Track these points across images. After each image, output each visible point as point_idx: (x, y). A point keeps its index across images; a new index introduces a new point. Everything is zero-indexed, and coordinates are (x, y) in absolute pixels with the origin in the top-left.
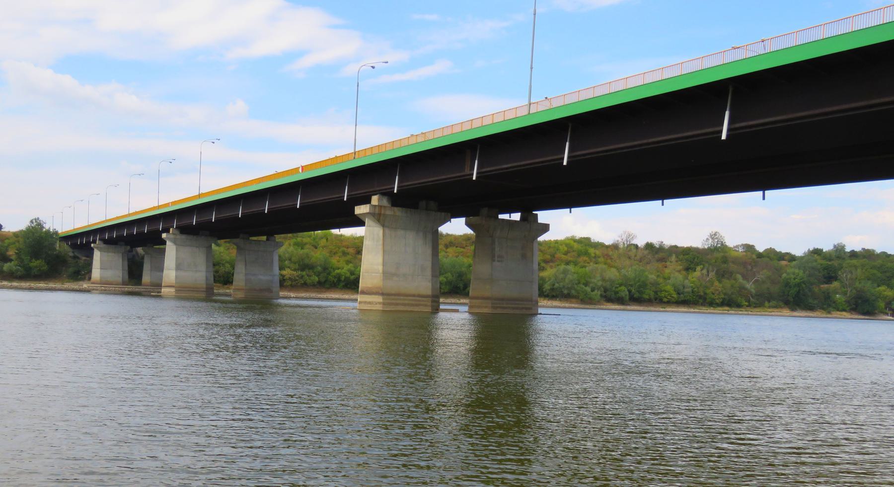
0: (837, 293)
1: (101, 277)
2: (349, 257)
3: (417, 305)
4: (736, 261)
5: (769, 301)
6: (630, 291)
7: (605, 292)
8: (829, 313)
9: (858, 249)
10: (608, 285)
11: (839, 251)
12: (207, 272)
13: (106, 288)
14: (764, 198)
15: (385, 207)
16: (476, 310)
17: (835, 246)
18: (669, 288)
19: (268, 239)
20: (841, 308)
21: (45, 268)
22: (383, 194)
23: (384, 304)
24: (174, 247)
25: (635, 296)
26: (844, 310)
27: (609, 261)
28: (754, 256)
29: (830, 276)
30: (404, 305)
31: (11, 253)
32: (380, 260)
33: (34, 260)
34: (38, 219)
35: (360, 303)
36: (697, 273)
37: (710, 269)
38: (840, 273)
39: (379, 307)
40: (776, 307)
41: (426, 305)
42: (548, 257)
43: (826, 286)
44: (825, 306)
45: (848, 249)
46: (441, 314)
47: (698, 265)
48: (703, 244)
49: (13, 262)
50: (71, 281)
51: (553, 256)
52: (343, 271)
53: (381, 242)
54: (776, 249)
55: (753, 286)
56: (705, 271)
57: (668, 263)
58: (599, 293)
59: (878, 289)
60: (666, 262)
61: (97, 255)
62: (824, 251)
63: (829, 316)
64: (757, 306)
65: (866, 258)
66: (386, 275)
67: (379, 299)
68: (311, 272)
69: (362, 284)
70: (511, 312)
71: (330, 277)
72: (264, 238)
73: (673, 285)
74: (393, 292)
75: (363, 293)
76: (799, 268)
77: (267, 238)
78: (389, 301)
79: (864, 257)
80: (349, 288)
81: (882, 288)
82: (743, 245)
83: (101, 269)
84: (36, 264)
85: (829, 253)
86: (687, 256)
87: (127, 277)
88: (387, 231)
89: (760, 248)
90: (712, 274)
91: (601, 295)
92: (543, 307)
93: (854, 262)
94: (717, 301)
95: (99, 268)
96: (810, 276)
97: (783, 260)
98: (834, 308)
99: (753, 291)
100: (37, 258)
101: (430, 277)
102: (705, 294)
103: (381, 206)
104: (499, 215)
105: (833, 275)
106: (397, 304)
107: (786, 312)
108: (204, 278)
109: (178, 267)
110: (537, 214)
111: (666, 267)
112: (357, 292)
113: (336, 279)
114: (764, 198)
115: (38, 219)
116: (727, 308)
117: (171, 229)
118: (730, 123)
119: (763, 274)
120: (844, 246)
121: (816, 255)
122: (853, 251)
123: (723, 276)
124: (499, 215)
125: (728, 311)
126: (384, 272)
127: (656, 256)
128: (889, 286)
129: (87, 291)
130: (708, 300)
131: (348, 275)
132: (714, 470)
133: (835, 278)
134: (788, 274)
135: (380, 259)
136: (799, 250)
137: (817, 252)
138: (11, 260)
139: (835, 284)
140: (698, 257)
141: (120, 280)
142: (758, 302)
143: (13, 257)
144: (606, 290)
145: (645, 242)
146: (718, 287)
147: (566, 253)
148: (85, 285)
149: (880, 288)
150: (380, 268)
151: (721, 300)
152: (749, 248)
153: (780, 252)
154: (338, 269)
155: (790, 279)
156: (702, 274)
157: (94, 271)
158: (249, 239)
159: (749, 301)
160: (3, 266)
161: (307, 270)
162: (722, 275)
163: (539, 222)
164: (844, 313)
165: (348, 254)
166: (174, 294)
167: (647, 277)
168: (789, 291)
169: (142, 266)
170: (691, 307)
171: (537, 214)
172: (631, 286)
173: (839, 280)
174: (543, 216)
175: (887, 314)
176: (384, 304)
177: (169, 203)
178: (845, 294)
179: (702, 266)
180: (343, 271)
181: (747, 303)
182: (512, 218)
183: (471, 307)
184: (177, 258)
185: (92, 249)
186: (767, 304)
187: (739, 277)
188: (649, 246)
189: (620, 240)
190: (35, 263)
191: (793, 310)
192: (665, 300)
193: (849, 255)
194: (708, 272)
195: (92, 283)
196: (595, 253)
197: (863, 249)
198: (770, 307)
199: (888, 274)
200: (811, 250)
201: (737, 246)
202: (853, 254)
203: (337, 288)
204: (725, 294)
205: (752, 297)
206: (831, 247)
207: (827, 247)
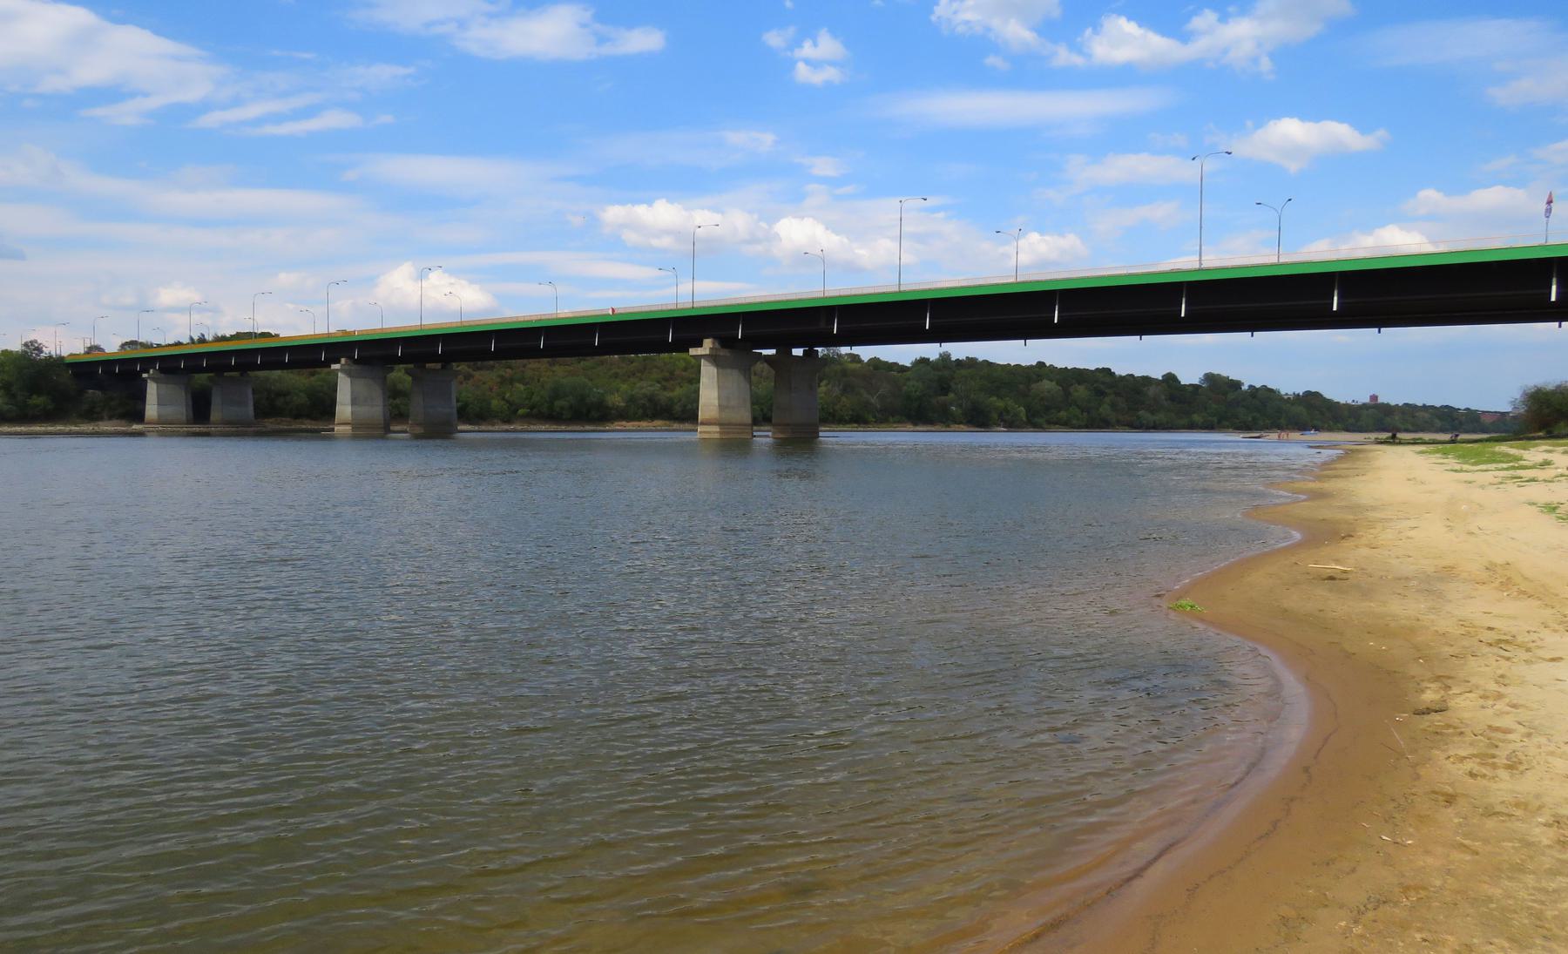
0: (952, 405)
1: (159, 416)
3: (741, 433)
5: (893, 416)
6: (762, 410)
8: (948, 426)
12: (384, 406)
13: (167, 428)
16: (776, 436)
17: (940, 355)
19: (443, 367)
23: (720, 433)
24: (348, 380)
26: (961, 423)
29: (944, 388)
32: (716, 394)
33: (35, 396)
34: (36, 342)
35: (701, 432)
38: (952, 384)
40: (899, 422)
42: (667, 374)
43: (943, 398)
44: (944, 420)
45: (953, 359)
50: (86, 421)
51: (672, 373)
53: (716, 379)
63: (948, 429)
66: (721, 407)
67: (716, 429)
72: (439, 366)
75: (702, 424)
88: (721, 370)
93: (964, 372)
104: (793, 350)
107: (910, 427)
109: (354, 402)
112: (334, 424)
116: (856, 425)
118: (1059, 313)
120: (950, 355)
124: (793, 350)
129: (140, 434)
132: (243, 775)
135: (715, 394)
139: (951, 395)
141: (184, 418)
147: (685, 369)
148: (136, 427)
150: (716, 402)
157: (148, 407)
159: (875, 417)
162: (847, 389)
163: (866, 361)
164: (962, 426)
175: (999, 425)
176: (720, 433)
178: (960, 406)
181: (874, 420)
183: (774, 433)
184: (352, 392)
185: (145, 381)
186: (891, 419)
190: (38, 400)
191: (915, 424)
197: (967, 358)
198: (895, 422)
204: (853, 410)
206: (938, 356)
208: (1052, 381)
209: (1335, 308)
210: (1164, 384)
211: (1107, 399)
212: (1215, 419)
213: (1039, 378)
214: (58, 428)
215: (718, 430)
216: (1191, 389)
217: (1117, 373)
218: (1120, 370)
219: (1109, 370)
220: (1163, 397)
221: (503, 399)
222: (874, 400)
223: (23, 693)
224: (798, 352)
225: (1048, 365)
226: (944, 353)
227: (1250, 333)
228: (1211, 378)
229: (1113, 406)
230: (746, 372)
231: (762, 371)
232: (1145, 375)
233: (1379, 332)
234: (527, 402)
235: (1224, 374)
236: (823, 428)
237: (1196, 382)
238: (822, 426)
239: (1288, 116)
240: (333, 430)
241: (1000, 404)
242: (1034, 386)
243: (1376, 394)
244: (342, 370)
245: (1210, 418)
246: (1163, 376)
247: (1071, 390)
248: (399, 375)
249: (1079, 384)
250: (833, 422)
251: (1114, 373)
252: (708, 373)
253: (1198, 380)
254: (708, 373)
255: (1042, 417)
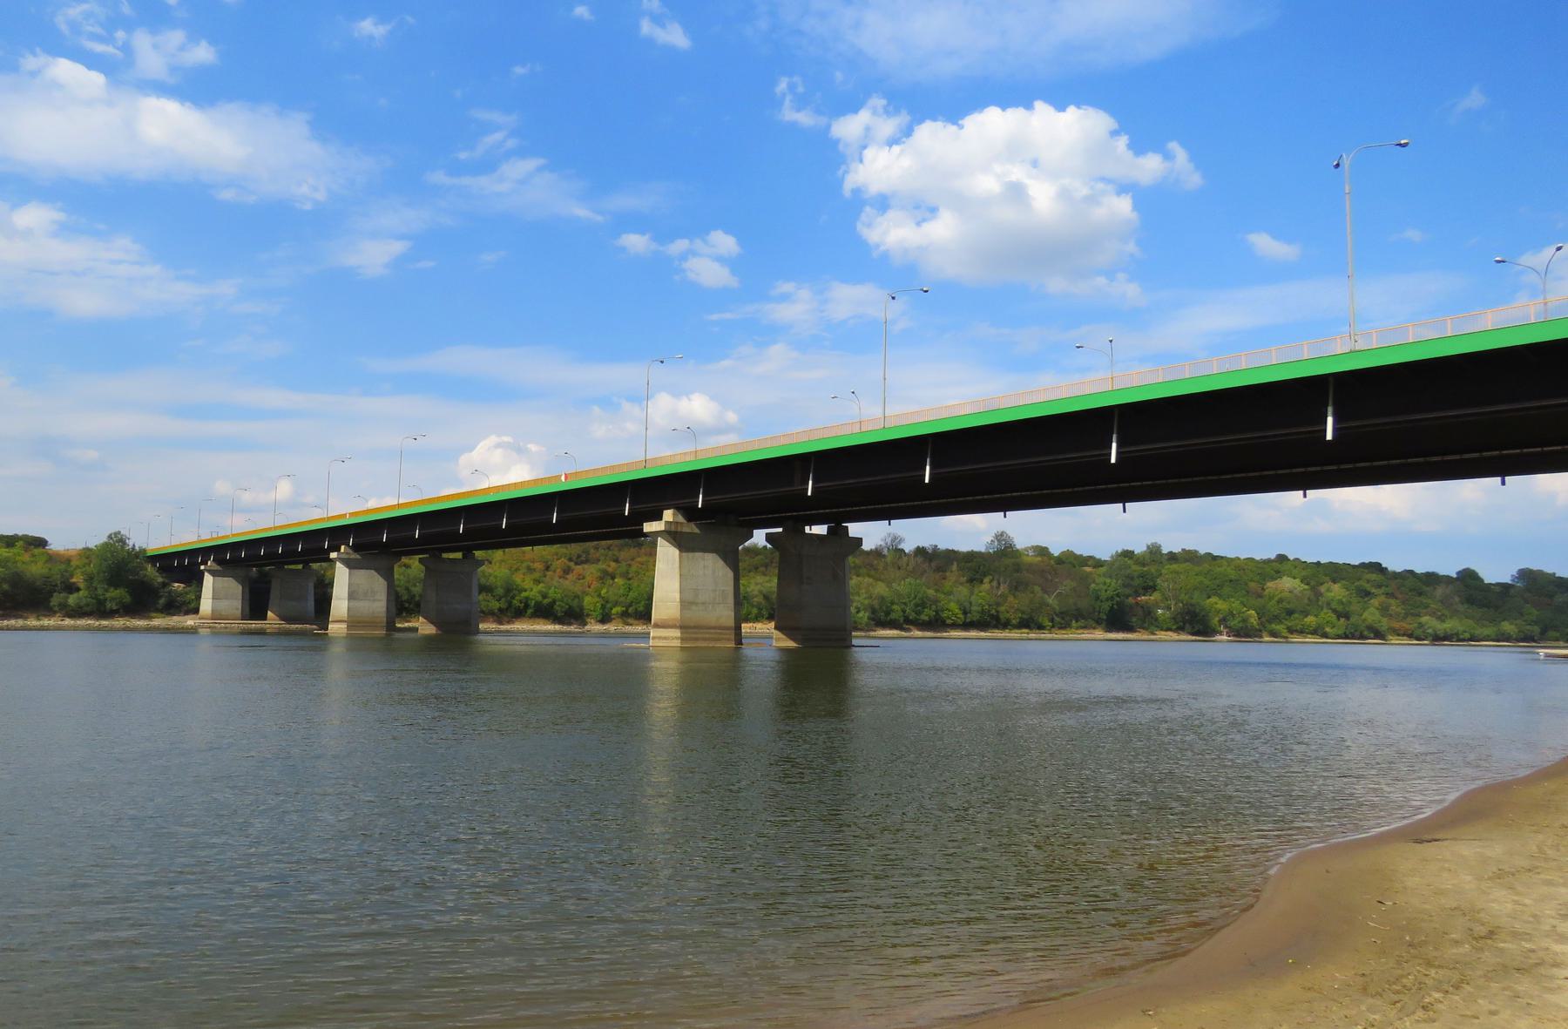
2: (537, 575)
3: (719, 640)
4: (1030, 568)
6: (904, 611)
7: (873, 613)
9: (1177, 550)
10: (876, 603)
11: (1154, 551)
14: (1125, 511)
15: (681, 523)
17: (1148, 547)
18: (953, 606)
19: (465, 556)
20: (1165, 627)
21: (128, 599)
22: (678, 508)
25: (911, 618)
26: (1168, 629)
27: (873, 573)
28: (1052, 562)
30: (705, 639)
31: (78, 579)
34: (119, 532)
35: (654, 638)
36: (986, 586)
37: (1001, 580)
38: (1159, 581)
39: (677, 643)
41: (729, 640)
45: (1165, 551)
46: (481, 637)
47: (985, 576)
48: (987, 548)
49: (81, 593)
52: (532, 593)
54: (1076, 552)
55: (1056, 602)
56: (995, 584)
57: (948, 574)
58: (867, 614)
59: (1208, 601)
60: (946, 571)
61: (208, 580)
62: (1136, 553)
63: (1153, 637)
64: (1064, 626)
65: (1188, 561)
66: (685, 604)
68: (489, 597)
69: (656, 615)
70: (704, 644)
71: (515, 602)
73: (958, 602)
74: (692, 624)
75: (657, 626)
76: (1110, 577)
77: (463, 555)
78: (688, 636)
79: (1186, 561)
80: (538, 617)
81: (1214, 599)
82: (1033, 547)
83: (213, 599)
84: (116, 594)
85: (1143, 555)
86: (970, 564)
87: (247, 609)
89: (1056, 551)
90: (1003, 589)
91: (869, 618)
92: (857, 637)
94: (1014, 622)
95: (211, 597)
96: (1125, 586)
97: (1087, 565)
98: (1157, 627)
99: (1057, 608)
100: (116, 586)
101: (732, 606)
102: (998, 612)
103: (677, 523)
105: (1151, 584)
106: (696, 639)
108: (385, 609)
109: (352, 596)
110: (847, 527)
111: (944, 579)
113: (523, 604)
114: (1125, 511)
115: (119, 532)
116: (1026, 631)
117: (343, 547)
119: (1067, 585)
120: (1160, 546)
121: (1127, 559)
122: (1171, 552)
123: (1016, 588)
125: (1028, 633)
126: (682, 601)
127: (933, 564)
128: (1220, 596)
130: (1003, 620)
131: (540, 598)
133: (1153, 588)
134: (1097, 584)
136: (1105, 554)
137: (1127, 554)
138: (78, 590)
139: (1155, 596)
140: (984, 565)
142: (1063, 622)
143: (82, 586)
144: (874, 611)
145: (916, 546)
146: (1012, 606)
149: (1211, 600)
150: (677, 596)
151: (1018, 620)
152: (1042, 551)
153: (1081, 555)
154: (526, 591)
155: (1100, 590)
156: (992, 587)
158: (440, 557)
159: (1052, 620)
160: (68, 598)
161: (485, 594)
162: (1016, 587)
163: (850, 535)
165: (534, 570)
166: (345, 631)
167: (925, 592)
168: (1100, 607)
169: (268, 591)
170: (939, 632)
171: (847, 527)
172: (905, 604)
173: (1159, 590)
174: (855, 529)
177: (346, 514)
179: (991, 577)
180: (532, 593)
182: (812, 532)
187: (1037, 589)
188: (920, 551)
189: (883, 543)
190: (115, 593)
192: (949, 622)
193: (1166, 557)
194: (999, 584)
195: (200, 619)
196: (854, 562)
197: (1183, 550)
198: (1077, 628)
199: (1217, 582)
200: (1119, 552)
201: (1026, 549)
202: (1172, 557)
203: (524, 616)
205: (1056, 615)
207: (1139, 548)
208: (1295, 578)
209: (1329, 436)
210: (1458, 583)
211: (1375, 602)
212: (1536, 629)
213: (1278, 574)
214: (89, 622)
215: (679, 635)
216: (1498, 589)
217: (1389, 569)
218: (1170, 545)
219: (1380, 565)
220: (1457, 599)
221: (599, 595)
222: (1051, 600)
223: (390, 952)
224: (820, 530)
225: (1291, 558)
226: (1152, 544)
227: (1301, 492)
228: (1527, 575)
229: (1384, 610)
230: (732, 559)
231: (908, 565)
232: (1430, 570)
233: (1503, 483)
234: (622, 599)
235: (1548, 569)
236: (859, 634)
237: (1507, 579)
238: (483, 621)
239: (1133, 203)
240: (646, 636)
241: (1222, 605)
242: (1270, 584)
243: (1000, 531)
244: (339, 559)
245: (1528, 627)
246: (1458, 573)
247: (1323, 589)
248: (412, 568)
249: (1334, 581)
250: (996, 627)
251: (1386, 569)
252: (667, 555)
253: (1510, 578)
254: (667, 555)
255: (1280, 622)
